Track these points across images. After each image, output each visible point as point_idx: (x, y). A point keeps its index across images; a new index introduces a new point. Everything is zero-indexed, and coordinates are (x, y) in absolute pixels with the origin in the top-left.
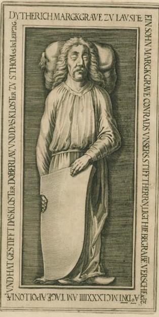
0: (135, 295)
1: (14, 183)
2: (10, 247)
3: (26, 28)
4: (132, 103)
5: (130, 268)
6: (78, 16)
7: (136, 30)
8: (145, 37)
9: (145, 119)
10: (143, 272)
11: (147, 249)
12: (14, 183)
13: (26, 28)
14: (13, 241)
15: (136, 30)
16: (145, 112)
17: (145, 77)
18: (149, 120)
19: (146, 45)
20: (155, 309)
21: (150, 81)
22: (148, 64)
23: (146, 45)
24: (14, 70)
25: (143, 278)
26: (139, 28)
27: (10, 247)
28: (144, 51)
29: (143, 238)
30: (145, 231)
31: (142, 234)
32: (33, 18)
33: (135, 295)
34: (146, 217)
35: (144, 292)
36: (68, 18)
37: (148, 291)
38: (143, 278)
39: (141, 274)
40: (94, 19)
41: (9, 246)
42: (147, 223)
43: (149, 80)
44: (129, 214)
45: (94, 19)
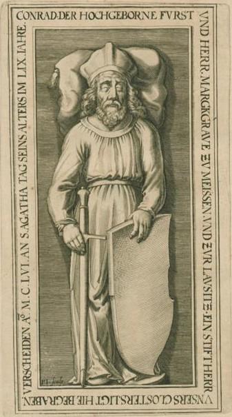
0: (29, 318)
1: (201, 30)
4: (185, 137)
5: (189, 298)
6: (206, 113)
7: (188, 29)
9: (46, 18)
12: (204, 235)
14: (204, 348)
15: (188, 29)
16: (36, 18)
18: (46, 404)
20: (196, 386)
21: (54, 404)
24: (206, 346)
26: (192, 27)
27: (208, 341)
29: (68, 398)
31: (73, 397)
32: (204, 185)
33: (29, 318)
36: (203, 59)
40: (205, 281)
43: (56, 403)
45: (205, 281)
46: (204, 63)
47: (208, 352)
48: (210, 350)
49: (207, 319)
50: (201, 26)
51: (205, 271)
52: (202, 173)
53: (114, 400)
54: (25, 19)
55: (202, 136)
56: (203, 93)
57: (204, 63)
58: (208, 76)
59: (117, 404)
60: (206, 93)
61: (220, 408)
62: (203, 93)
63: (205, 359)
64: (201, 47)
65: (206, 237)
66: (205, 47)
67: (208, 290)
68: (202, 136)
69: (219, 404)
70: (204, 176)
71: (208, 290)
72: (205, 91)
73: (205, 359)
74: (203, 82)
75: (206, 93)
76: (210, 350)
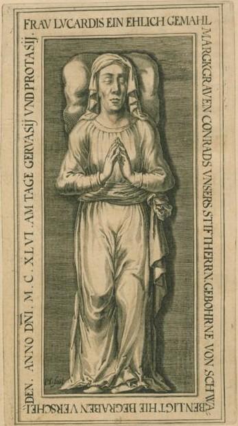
2: (209, 218)
3: (45, 40)
6: (207, 67)
8: (205, 310)
10: (206, 254)
11: (210, 144)
13: (45, 40)
17: (32, 184)
19: (31, 385)
22: (30, 76)
23: (122, 25)
25: (56, 408)
27: (209, 218)
28: (99, 18)
30: (34, 410)
34: (207, 61)
35: (127, 409)
37: (140, 16)
38: (56, 408)
39: (205, 258)
40: (205, 92)
41: (210, 218)
42: (134, 18)
44: (190, 203)
45: (205, 92)
46: (208, 264)
47: (208, 231)
48: (210, 228)
49: (112, 23)
50: (206, 331)
51: (26, 236)
52: (32, 300)
53: (178, 407)
54: (26, 70)
55: (44, 28)
56: (81, 26)
57: (208, 264)
58: (132, 276)
59: (182, 411)
60: (196, 20)
61: (223, 418)
62: (81, 26)
63: (25, 252)
64: (150, 404)
65: (31, 96)
66: (38, 409)
67: (30, 129)
68: (44, 28)
69: (223, 415)
70: (30, 297)
71: (30, 129)
72: (207, 150)
73: (25, 252)
74: (186, 23)
75: (196, 20)
76: (210, 228)
